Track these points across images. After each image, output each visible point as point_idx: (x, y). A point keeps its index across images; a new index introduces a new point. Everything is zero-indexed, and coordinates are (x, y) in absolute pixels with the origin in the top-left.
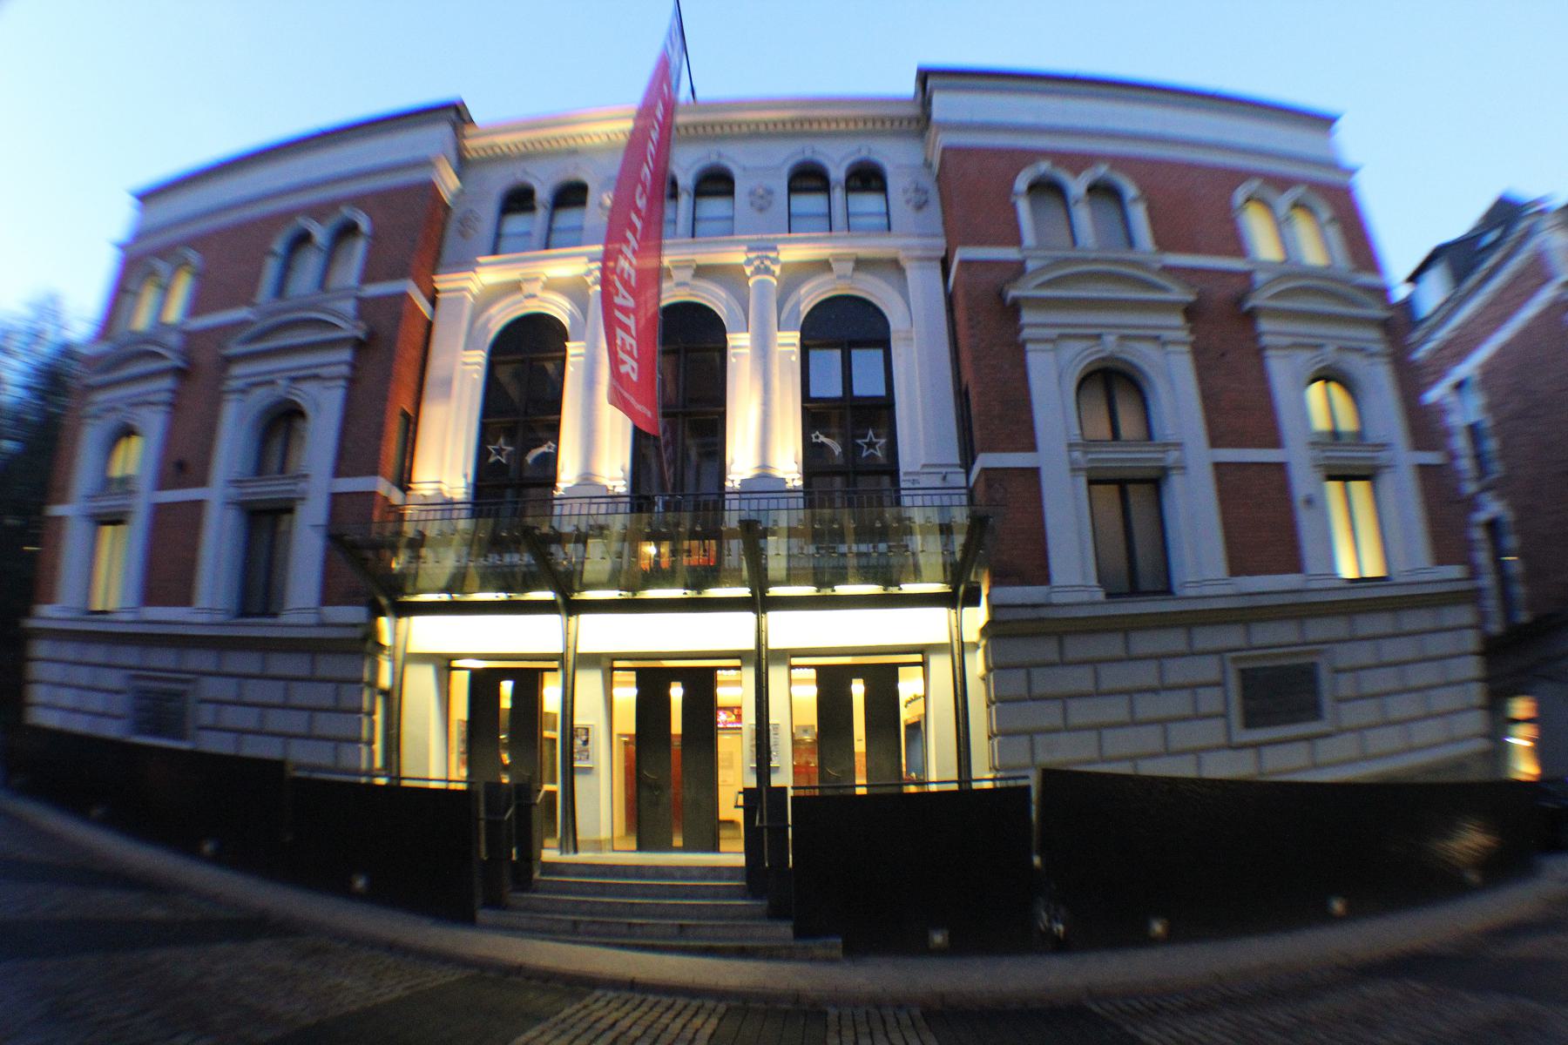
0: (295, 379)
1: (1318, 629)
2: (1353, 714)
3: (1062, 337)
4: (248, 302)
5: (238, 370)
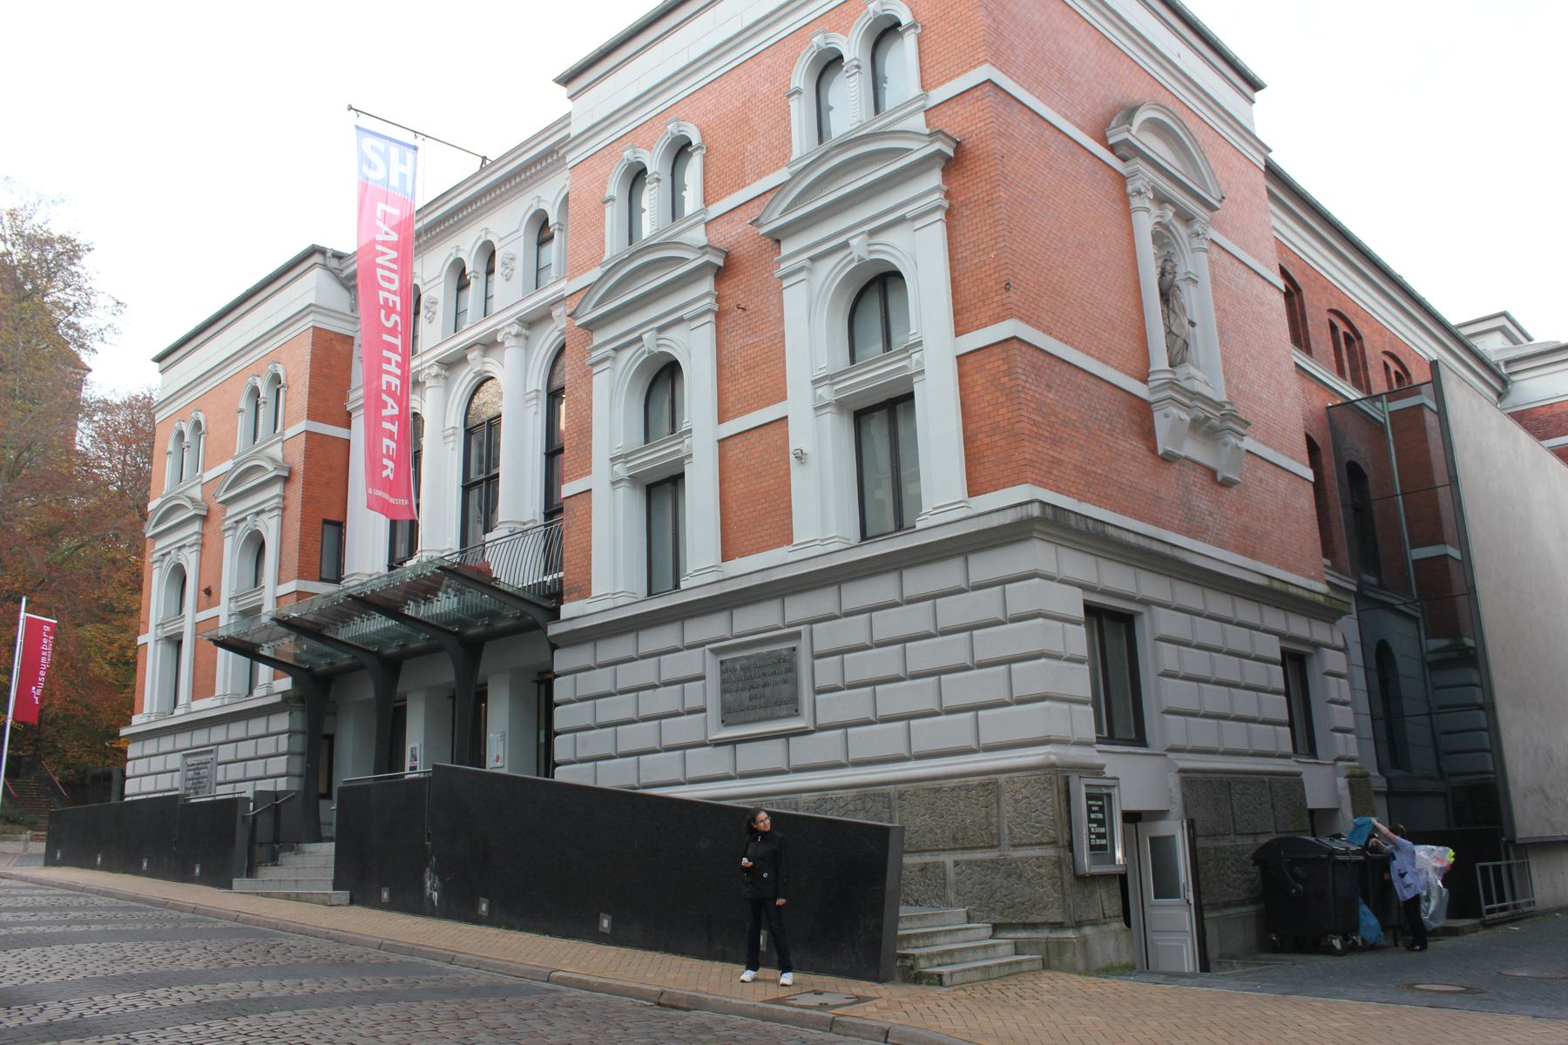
0: (661, 329)
1: (798, 608)
2: (834, 708)
3: (813, 259)
4: (784, 159)
5: (787, 248)
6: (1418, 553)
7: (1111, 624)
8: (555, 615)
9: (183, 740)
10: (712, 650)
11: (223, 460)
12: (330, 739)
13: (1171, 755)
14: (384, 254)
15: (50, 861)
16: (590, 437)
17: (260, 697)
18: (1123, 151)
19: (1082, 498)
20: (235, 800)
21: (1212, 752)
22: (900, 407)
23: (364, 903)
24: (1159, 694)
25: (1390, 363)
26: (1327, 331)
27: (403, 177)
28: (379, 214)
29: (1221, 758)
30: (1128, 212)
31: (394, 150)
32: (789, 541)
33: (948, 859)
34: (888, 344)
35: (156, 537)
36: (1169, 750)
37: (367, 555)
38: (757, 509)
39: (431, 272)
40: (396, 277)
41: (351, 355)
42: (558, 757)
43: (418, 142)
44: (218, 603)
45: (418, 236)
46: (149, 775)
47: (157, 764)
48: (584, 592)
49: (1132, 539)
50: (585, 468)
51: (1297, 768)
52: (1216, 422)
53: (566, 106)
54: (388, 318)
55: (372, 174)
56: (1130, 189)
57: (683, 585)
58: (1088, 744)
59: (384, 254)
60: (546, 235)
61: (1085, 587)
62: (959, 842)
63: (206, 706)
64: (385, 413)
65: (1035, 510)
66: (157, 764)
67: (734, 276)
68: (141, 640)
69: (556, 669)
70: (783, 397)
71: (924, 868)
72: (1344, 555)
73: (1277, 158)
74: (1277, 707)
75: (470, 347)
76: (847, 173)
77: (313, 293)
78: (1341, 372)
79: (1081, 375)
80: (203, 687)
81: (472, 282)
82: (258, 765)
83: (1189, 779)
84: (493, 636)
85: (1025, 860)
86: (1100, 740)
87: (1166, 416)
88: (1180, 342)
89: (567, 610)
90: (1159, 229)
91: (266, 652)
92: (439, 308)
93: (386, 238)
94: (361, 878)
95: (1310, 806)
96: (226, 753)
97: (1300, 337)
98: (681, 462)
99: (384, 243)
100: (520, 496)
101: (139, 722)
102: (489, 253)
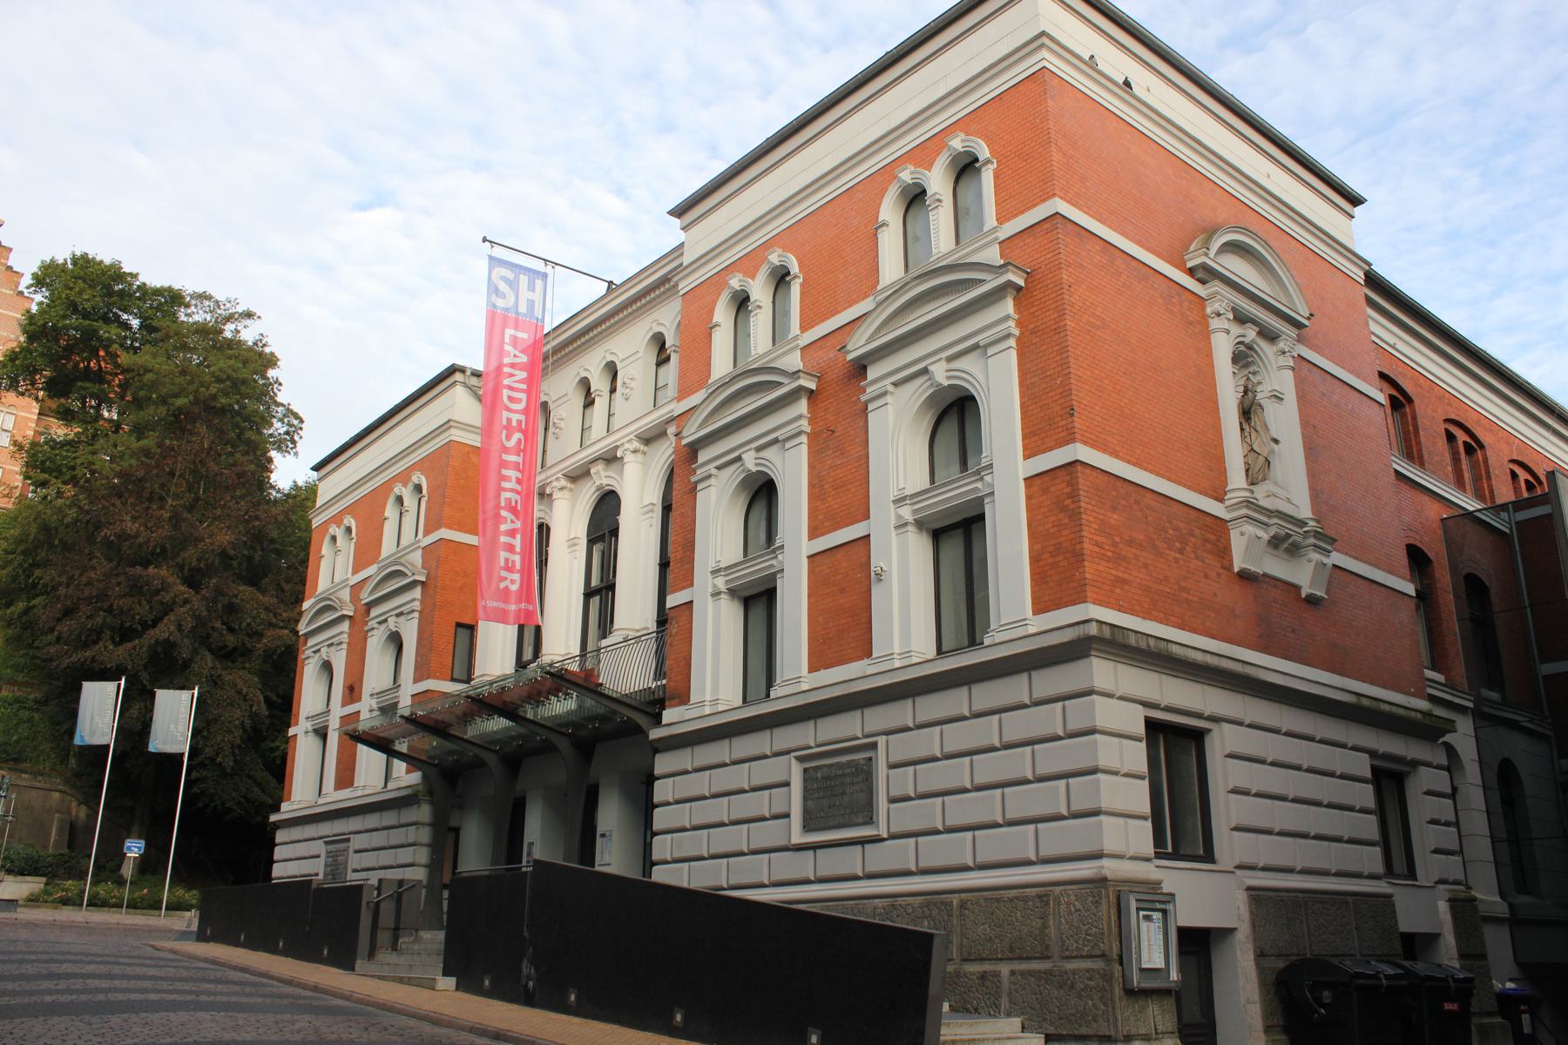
6: (1547, 669)
7: (1175, 743)
8: (657, 720)
9: (326, 829)
10: (797, 758)
11: (369, 564)
12: (456, 831)
13: (1239, 872)
14: (512, 375)
15: (201, 937)
16: (693, 552)
18: (1200, 275)
19: (1146, 615)
20: (361, 886)
21: (1290, 870)
22: (974, 527)
23: (467, 990)
24: (1226, 811)
25: (1518, 470)
26: (1442, 442)
27: (531, 303)
28: (507, 339)
29: (1299, 877)
30: (1206, 334)
31: (524, 280)
32: (869, 654)
33: (1005, 969)
34: (964, 465)
35: (309, 635)
36: (1239, 867)
37: (496, 656)
38: (845, 621)
40: (523, 396)
42: (656, 856)
43: (549, 269)
44: (359, 699)
45: (546, 358)
46: (295, 860)
47: (302, 850)
48: (683, 698)
49: (1199, 657)
50: (688, 581)
51: (1387, 890)
52: (1297, 538)
53: (681, 237)
54: (508, 438)
55: (500, 303)
56: (1209, 310)
57: (773, 695)
58: (1148, 860)
59: (512, 375)
61: (1145, 704)
62: (1015, 954)
63: (346, 797)
64: (503, 527)
65: (1093, 630)
66: (302, 850)
67: (840, 389)
68: (292, 731)
69: (657, 772)
71: (983, 976)
72: (1460, 669)
73: (1381, 269)
74: (1369, 826)
75: (592, 462)
76: (925, 303)
78: (1460, 484)
79: (1148, 495)
80: (345, 777)
81: (597, 400)
82: (391, 859)
83: (1257, 896)
84: (599, 742)
85: (1074, 972)
86: (1158, 856)
87: (1242, 534)
88: (1261, 460)
89: (668, 715)
90: (1242, 348)
91: (402, 747)
93: (517, 360)
94: (470, 963)
95: (1404, 927)
96: (358, 842)
97: (1411, 449)
99: (513, 366)
100: (635, 605)
101: (287, 809)
102: (612, 370)
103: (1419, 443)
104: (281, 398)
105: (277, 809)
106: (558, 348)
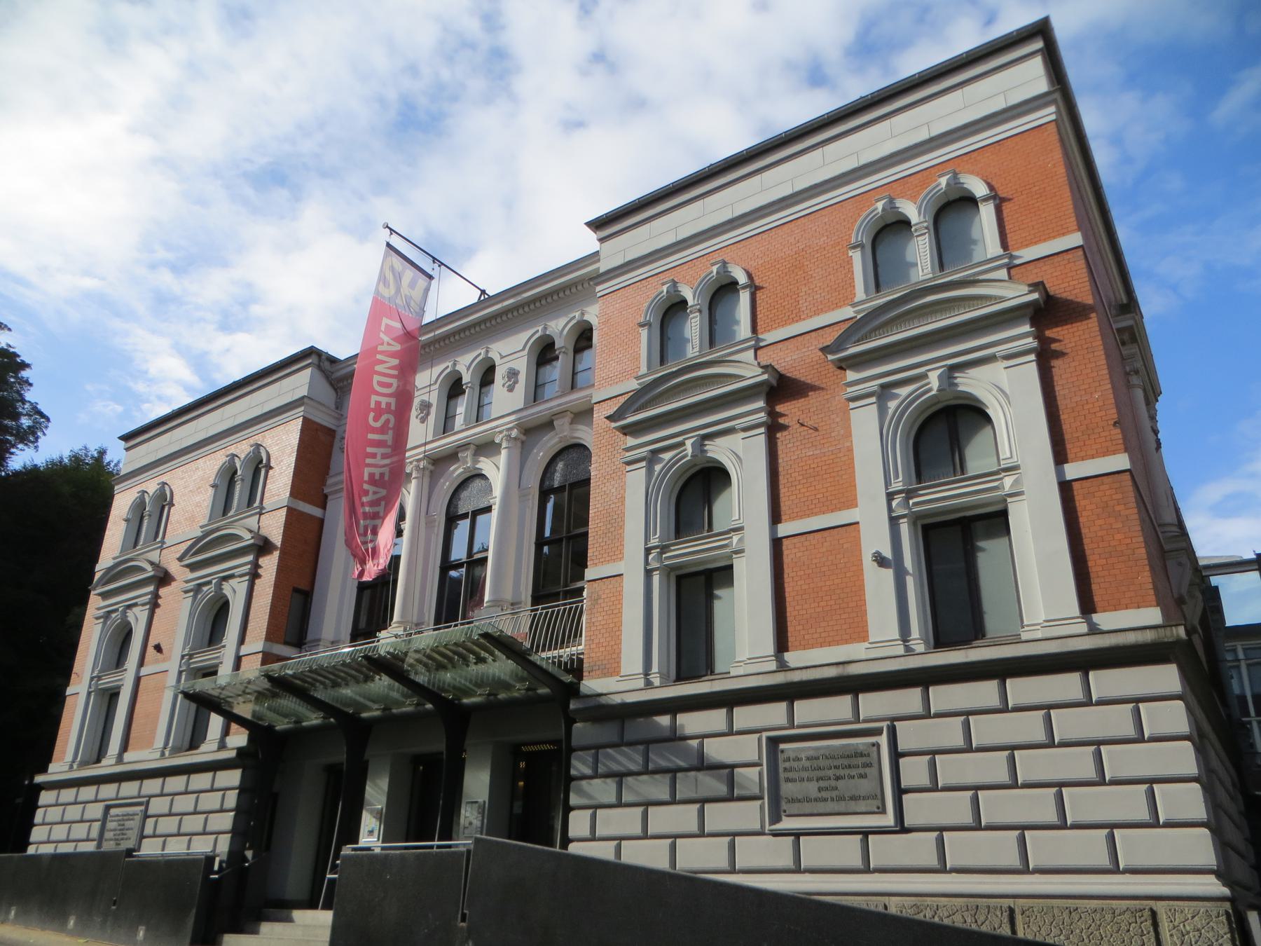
3: (884, 387)
14: (384, 362)
17: (208, 751)
31: (410, 273)
32: (864, 638)
39: (428, 382)
41: (332, 446)
42: (571, 834)
50: (616, 553)
60: (548, 356)
70: (851, 503)
77: (306, 387)
92: (433, 410)
98: (217, 666)
101: (58, 768)
103: (1072, 191)
104: (30, 395)
105: (44, 770)
106: (423, 344)
